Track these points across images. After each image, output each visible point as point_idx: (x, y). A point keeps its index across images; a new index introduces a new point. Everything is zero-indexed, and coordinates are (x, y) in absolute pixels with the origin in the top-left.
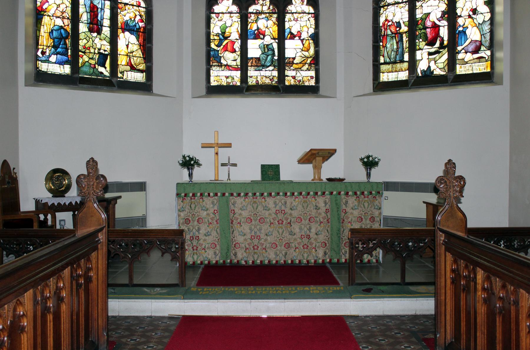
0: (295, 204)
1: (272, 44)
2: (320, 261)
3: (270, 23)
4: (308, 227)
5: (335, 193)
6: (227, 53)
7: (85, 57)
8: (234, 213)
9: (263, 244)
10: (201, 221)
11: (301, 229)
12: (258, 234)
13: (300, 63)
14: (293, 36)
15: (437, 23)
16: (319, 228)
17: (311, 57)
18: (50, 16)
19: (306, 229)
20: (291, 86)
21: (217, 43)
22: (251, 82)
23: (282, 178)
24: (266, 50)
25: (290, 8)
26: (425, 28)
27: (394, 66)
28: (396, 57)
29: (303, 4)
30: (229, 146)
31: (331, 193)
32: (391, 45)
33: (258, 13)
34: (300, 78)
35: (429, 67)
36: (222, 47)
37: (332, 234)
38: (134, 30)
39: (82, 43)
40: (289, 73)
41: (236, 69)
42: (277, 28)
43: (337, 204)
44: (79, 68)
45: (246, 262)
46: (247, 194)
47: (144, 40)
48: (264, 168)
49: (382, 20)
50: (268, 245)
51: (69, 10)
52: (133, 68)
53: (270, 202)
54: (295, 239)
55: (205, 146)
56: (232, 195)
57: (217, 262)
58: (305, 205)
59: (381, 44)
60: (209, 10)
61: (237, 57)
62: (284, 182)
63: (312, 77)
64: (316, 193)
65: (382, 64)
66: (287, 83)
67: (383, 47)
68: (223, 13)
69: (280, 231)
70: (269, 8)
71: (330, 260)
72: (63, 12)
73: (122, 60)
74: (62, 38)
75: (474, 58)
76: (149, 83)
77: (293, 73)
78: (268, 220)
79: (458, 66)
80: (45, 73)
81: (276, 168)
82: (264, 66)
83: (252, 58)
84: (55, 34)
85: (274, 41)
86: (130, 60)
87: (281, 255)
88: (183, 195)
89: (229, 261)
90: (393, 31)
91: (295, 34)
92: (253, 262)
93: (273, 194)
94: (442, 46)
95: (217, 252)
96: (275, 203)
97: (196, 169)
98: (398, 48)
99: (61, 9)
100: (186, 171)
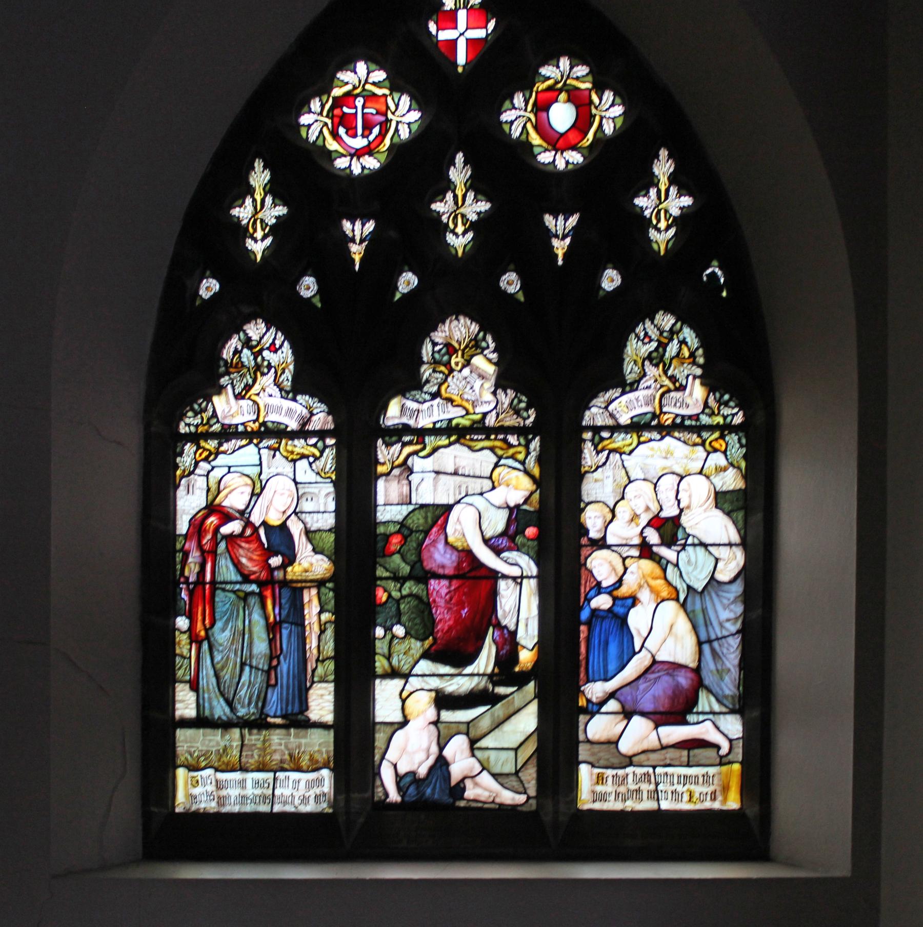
26: (423, 575)
27: (254, 738)
35: (441, 764)
98: (274, 655)
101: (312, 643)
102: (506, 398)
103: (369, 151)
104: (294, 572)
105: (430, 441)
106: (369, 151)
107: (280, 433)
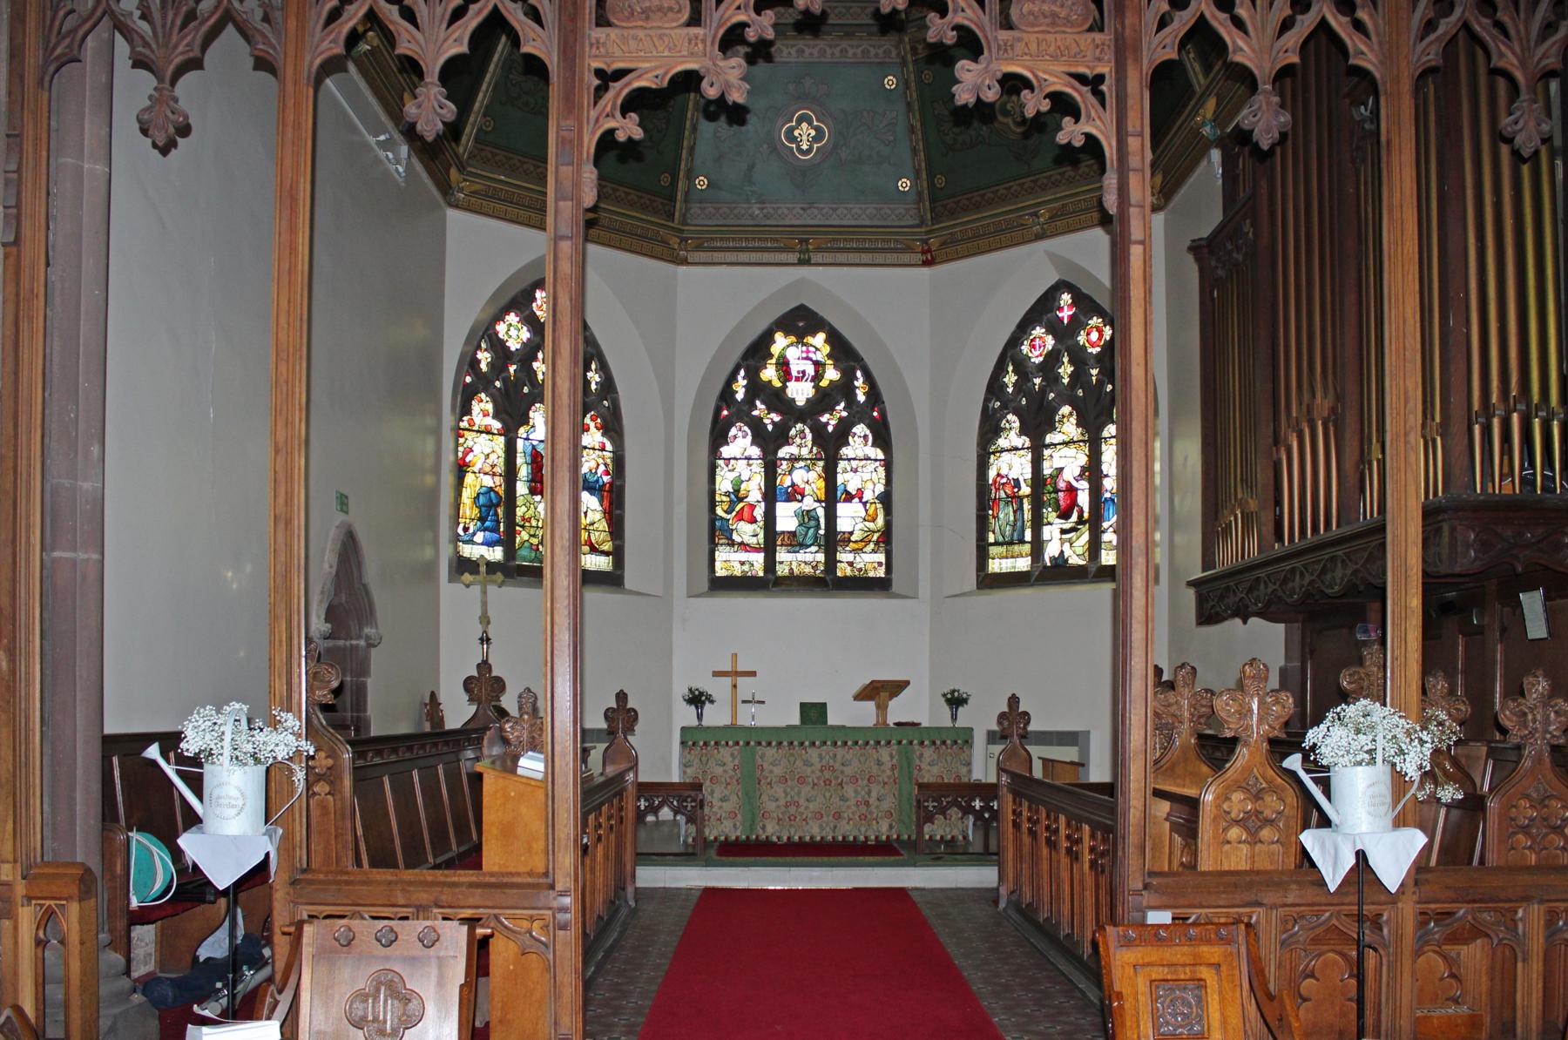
0: (848, 757)
1: (815, 509)
2: (884, 838)
3: (812, 475)
4: (866, 789)
5: (904, 742)
6: (742, 523)
7: (523, 533)
8: (762, 770)
9: (803, 814)
10: (715, 780)
11: (856, 792)
12: (796, 798)
13: (861, 541)
14: (849, 498)
15: (1075, 484)
16: (882, 791)
17: (878, 531)
18: (474, 473)
19: (863, 793)
20: (846, 578)
21: (725, 508)
22: (782, 570)
23: (830, 722)
24: (806, 520)
25: (845, 451)
26: (1056, 491)
27: (1010, 548)
28: (1012, 535)
29: (866, 445)
30: (753, 674)
31: (900, 743)
32: (1006, 514)
33: (794, 459)
34: (862, 565)
35: (1062, 552)
36: (734, 513)
37: (900, 801)
38: (595, 489)
39: (520, 511)
40: (844, 556)
41: (757, 550)
42: (823, 484)
43: (907, 758)
44: (516, 551)
45: (778, 838)
46: (780, 744)
47: (611, 503)
48: (805, 708)
49: (992, 474)
50: (810, 815)
51: (502, 460)
52: (594, 550)
53: (813, 754)
54: (848, 807)
55: (716, 674)
56: (759, 744)
57: (737, 838)
58: (863, 759)
59: (990, 512)
60: (714, 453)
61: (758, 530)
62: (833, 728)
63: (880, 564)
64: (878, 743)
65: (992, 544)
66: (839, 574)
67: (994, 517)
68: (735, 459)
69: (828, 795)
70: (811, 452)
71: (898, 837)
72: (493, 466)
74: (491, 506)
76: (619, 572)
77: (850, 557)
78: (810, 780)
79: (1103, 551)
80: (468, 560)
81: (821, 708)
82: (803, 546)
83: (783, 532)
84: (482, 500)
85: (818, 504)
86: (589, 536)
87: (828, 829)
88: (690, 743)
89: (754, 837)
90: (1009, 492)
91: (854, 493)
92: (789, 838)
93: (817, 743)
94: (1081, 521)
95: (738, 824)
96: (820, 756)
98: (1015, 520)
99: (490, 461)
101: (1026, 517)
102: (1080, 430)
103: (1041, 355)
104: (1021, 493)
105: (1058, 447)
106: (1041, 355)
107: (1016, 449)
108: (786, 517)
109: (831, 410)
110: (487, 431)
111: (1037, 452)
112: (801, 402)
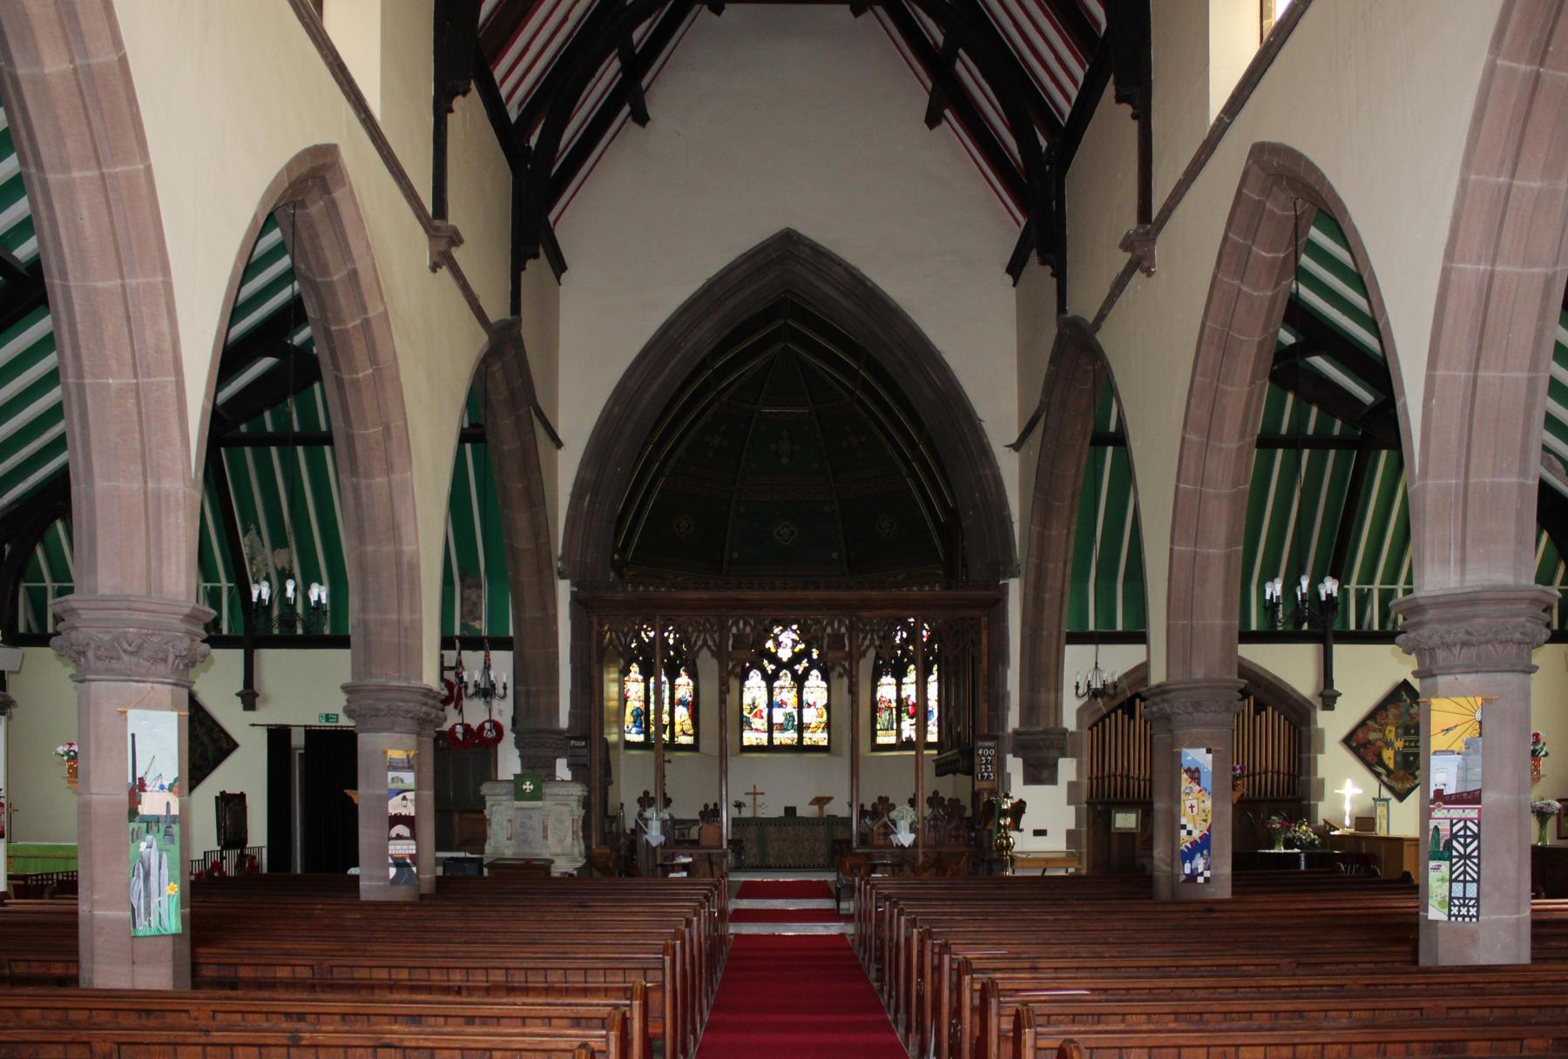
14: (809, 706)
22: (776, 742)
26: (908, 705)
30: (763, 794)
33: (782, 688)
40: (807, 735)
52: (685, 734)
53: (790, 828)
73: (678, 728)
75: (368, 970)
82: (786, 730)
97: (743, 809)
100: (737, 809)
108: (779, 716)
109: (800, 663)
110: (637, 681)
111: (899, 685)
112: (785, 659)
